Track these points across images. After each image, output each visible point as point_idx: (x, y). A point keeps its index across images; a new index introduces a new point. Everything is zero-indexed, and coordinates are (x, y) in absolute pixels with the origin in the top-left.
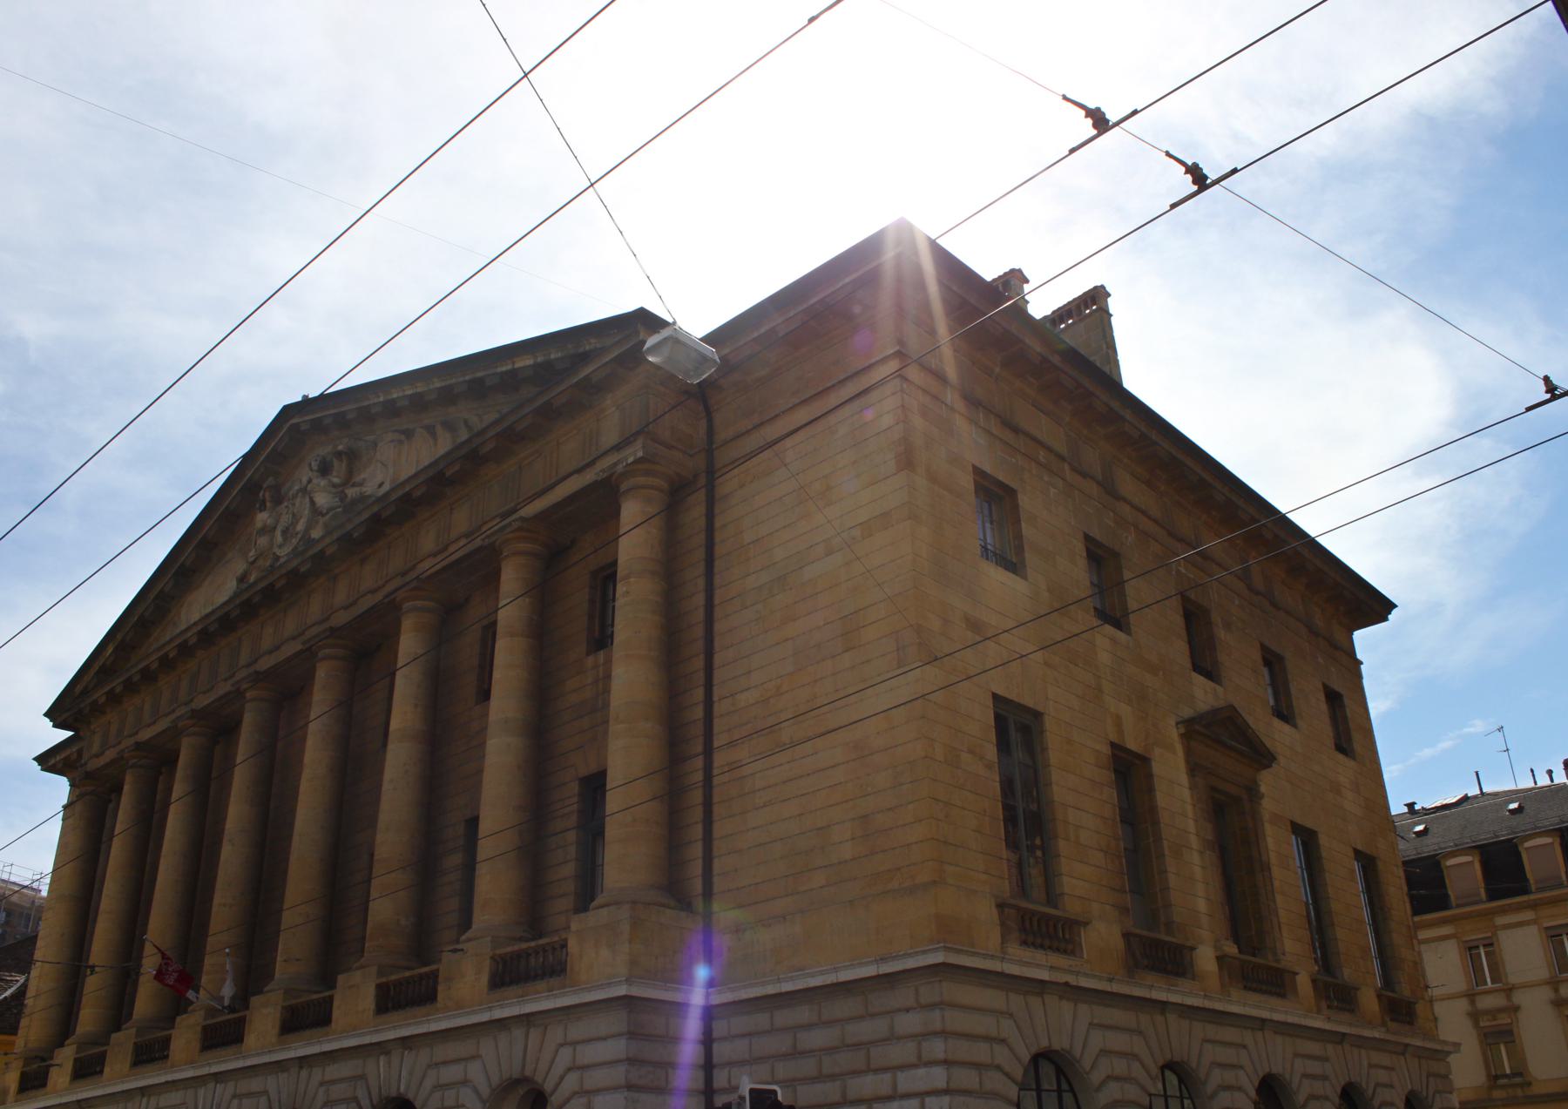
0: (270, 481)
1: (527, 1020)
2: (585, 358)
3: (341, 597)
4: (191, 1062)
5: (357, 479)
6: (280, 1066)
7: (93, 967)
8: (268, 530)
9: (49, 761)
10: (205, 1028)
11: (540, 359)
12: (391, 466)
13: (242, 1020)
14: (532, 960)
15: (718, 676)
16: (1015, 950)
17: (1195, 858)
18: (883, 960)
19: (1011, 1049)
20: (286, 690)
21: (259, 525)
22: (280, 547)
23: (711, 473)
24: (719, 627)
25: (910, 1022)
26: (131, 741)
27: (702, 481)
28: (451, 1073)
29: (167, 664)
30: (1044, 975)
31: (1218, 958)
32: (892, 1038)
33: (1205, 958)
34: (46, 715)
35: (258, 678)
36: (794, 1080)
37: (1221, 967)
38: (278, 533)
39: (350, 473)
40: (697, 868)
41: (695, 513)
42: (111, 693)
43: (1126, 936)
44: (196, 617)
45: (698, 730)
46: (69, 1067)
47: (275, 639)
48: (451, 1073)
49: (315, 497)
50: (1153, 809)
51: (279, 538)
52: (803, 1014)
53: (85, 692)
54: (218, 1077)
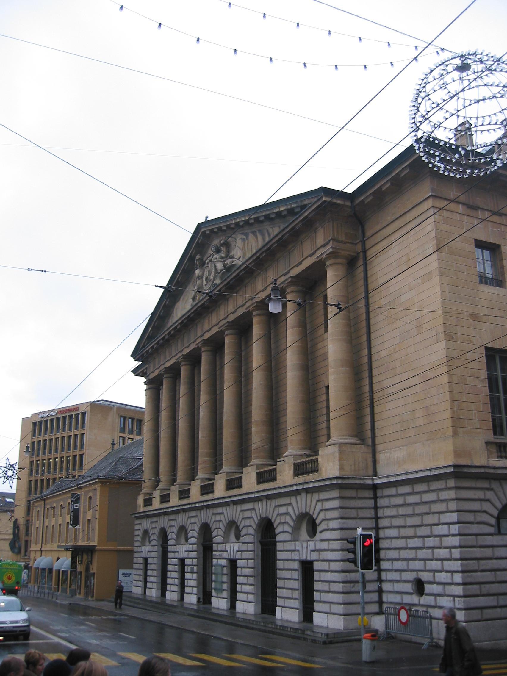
0: (198, 257)
2: (303, 207)
3: (231, 308)
5: (232, 254)
7: (144, 481)
8: (200, 277)
9: (136, 372)
10: (201, 486)
11: (289, 207)
12: (243, 249)
13: (213, 484)
14: (308, 466)
15: (373, 343)
20: (216, 345)
21: (197, 275)
22: (206, 285)
23: (365, 251)
24: (372, 322)
27: (361, 255)
28: (283, 510)
34: (131, 356)
35: (206, 342)
36: (405, 515)
38: (204, 279)
39: (228, 252)
40: (368, 426)
44: (179, 316)
45: (366, 367)
46: (158, 498)
47: (210, 326)
48: (283, 510)
49: (209, 275)
51: (205, 282)
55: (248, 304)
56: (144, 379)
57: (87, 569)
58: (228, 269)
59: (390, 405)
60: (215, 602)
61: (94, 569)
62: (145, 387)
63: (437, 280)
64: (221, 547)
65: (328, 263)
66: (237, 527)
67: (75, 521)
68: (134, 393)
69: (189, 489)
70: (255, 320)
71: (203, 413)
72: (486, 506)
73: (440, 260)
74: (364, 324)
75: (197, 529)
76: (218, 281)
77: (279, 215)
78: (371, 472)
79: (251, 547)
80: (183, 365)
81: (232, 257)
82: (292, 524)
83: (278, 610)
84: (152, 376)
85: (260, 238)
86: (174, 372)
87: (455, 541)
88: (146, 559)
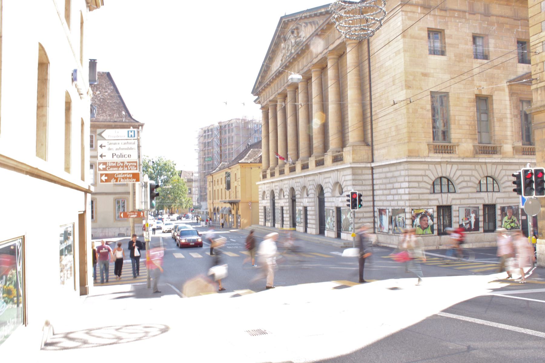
1: (337, 170)
4: (288, 175)
6: (301, 177)
8: (284, 48)
16: (432, 155)
17: (509, 121)
18: (397, 159)
19: (429, 177)
25: (403, 173)
26: (268, 100)
29: (271, 82)
30: (439, 160)
31: (513, 147)
32: (400, 176)
33: (508, 148)
37: (513, 150)
39: (298, 33)
40: (369, 135)
41: (365, 47)
42: (262, 89)
43: (473, 146)
50: (493, 109)
52: (386, 169)
53: (258, 88)
54: (293, 178)
55: (309, 65)
56: (259, 106)
57: (237, 213)
58: (297, 44)
59: (380, 124)
60: (297, 228)
61: (240, 212)
62: (261, 111)
63: (402, 54)
64: (299, 200)
65: (347, 43)
66: (340, 186)
67: (228, 187)
68: (254, 113)
69: (284, 170)
70: (348, 49)
71: (351, 93)
72: (426, 179)
73: (404, 43)
74: (368, 78)
75: (288, 191)
76: (293, 51)
77: (321, 14)
78: (370, 160)
79: (313, 200)
80: (330, 59)
81: (300, 37)
82: (331, 187)
83: (326, 232)
84: (264, 104)
85: (313, 26)
86: (274, 102)
87: (407, 197)
88: (282, 207)
